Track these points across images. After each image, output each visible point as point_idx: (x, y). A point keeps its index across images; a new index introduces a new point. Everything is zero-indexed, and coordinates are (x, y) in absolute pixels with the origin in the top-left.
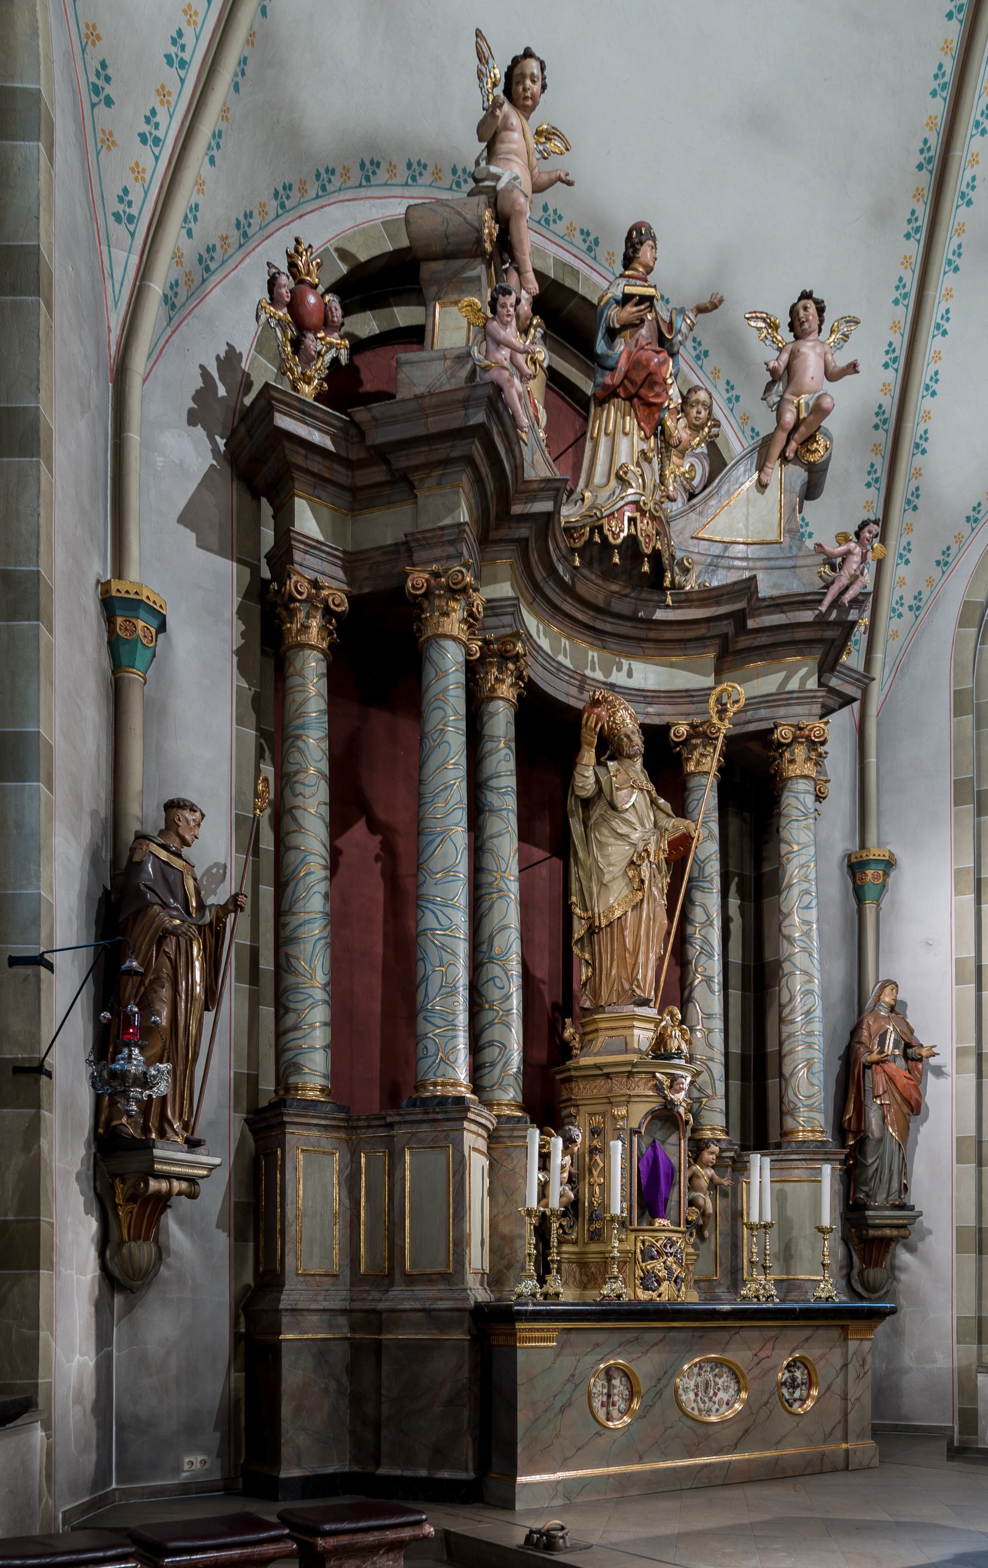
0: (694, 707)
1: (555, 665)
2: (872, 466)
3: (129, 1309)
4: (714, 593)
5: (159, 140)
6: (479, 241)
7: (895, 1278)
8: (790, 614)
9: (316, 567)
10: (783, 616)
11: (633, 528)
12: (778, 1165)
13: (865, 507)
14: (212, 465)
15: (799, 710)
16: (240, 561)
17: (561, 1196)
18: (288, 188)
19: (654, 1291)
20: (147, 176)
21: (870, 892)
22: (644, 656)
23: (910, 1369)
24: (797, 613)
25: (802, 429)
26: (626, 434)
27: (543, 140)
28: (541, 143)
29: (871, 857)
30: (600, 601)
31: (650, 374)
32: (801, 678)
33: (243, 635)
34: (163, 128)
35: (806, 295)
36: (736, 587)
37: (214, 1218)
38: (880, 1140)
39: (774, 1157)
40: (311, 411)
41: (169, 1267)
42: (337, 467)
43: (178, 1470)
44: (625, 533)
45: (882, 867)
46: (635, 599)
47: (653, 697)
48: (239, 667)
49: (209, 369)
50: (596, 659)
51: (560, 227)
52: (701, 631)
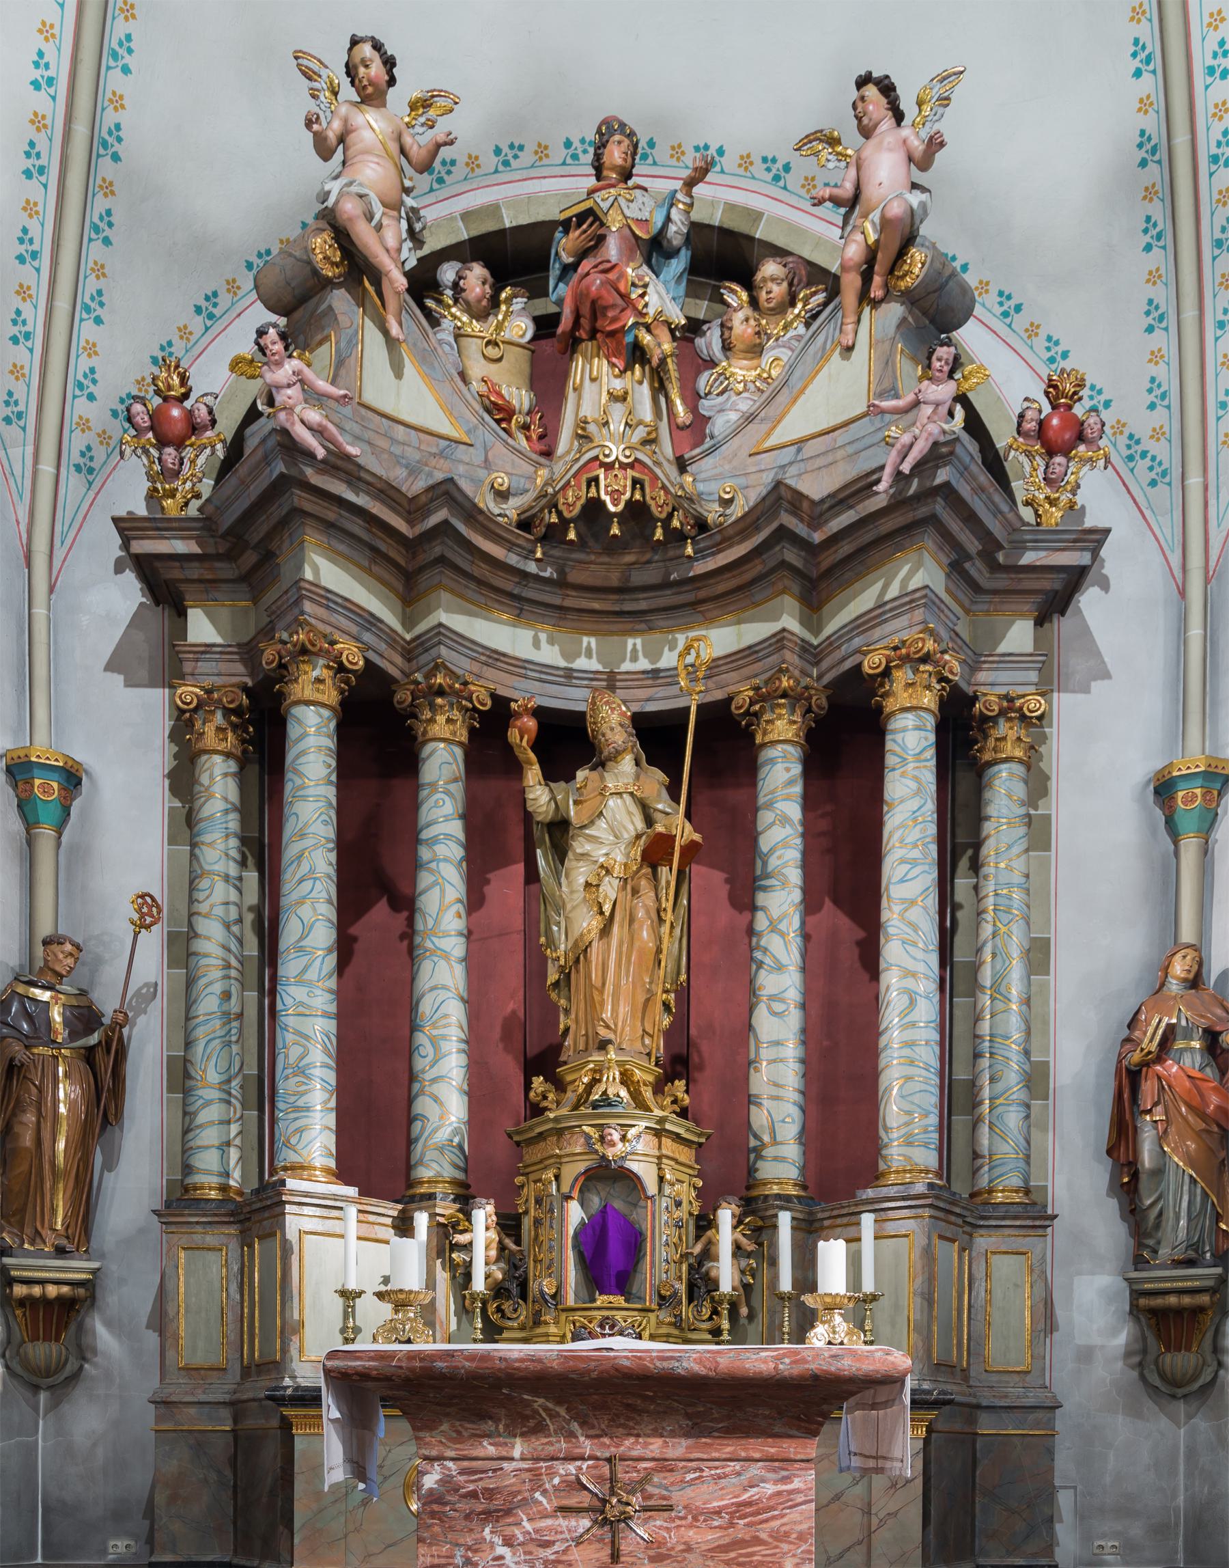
1: (561, 673)
3: (55, 1405)
4: (749, 520)
5: (30, 333)
6: (315, 272)
8: (860, 507)
10: (852, 512)
12: (362, 1217)
14: (141, 604)
18: (212, 297)
22: (710, 621)
24: (867, 502)
25: (880, 256)
27: (421, 111)
29: (1175, 774)
30: (614, 579)
31: (593, 302)
32: (903, 580)
33: (176, 756)
34: (30, 322)
35: (863, 82)
36: (768, 503)
37: (144, 1320)
38: (1158, 1172)
39: (361, 1207)
42: (218, 565)
43: (104, 1552)
44: (583, 501)
45: (1199, 782)
46: (664, 561)
48: (171, 789)
50: (639, 647)
52: (756, 568)
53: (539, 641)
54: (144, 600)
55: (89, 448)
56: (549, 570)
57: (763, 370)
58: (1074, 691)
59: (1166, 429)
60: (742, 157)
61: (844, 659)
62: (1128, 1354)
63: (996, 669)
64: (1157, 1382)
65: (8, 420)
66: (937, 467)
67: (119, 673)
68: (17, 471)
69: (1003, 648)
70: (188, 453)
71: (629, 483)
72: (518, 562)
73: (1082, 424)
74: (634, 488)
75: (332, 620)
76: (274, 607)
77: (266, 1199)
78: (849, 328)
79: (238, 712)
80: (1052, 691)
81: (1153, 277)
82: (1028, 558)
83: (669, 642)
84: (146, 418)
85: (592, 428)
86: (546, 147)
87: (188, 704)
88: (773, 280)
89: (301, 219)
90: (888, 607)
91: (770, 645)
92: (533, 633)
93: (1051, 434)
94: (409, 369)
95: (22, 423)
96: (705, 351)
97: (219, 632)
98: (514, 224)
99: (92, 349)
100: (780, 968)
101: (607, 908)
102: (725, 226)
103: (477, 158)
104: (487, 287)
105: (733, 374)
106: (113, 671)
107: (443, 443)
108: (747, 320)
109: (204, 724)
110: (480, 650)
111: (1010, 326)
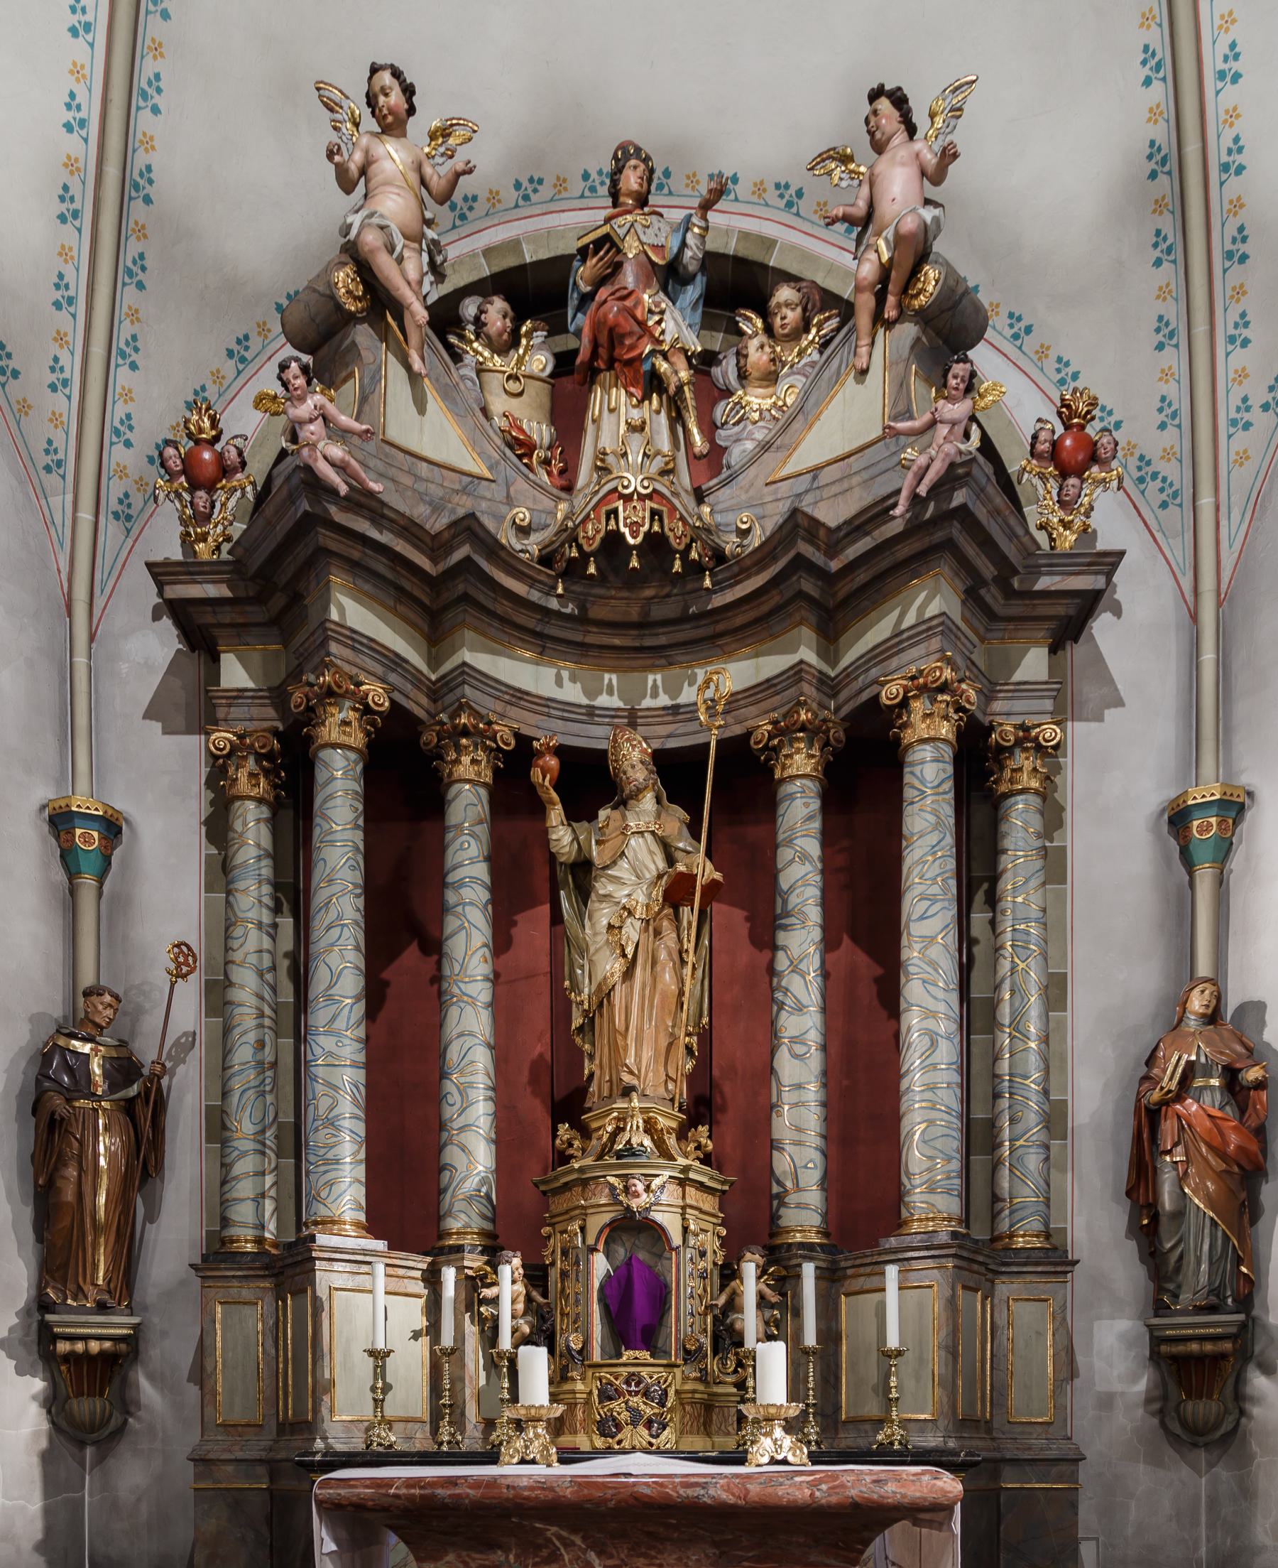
0: (778, 697)
3: (100, 1459)
7: (1242, 1412)
8: (876, 533)
9: (242, 716)
10: (868, 539)
11: (612, 522)
14: (178, 651)
15: (914, 653)
17: (513, 1333)
18: (243, 340)
19: (613, 1437)
20: (65, 419)
21: (1202, 854)
22: (728, 654)
23: (1265, 1547)
24: (883, 528)
25: (893, 274)
26: (611, 411)
28: (441, 145)
30: (634, 614)
31: (611, 330)
35: (874, 95)
36: (784, 531)
37: (186, 1373)
38: (1179, 1215)
40: (197, 569)
41: (139, 1419)
44: (602, 534)
45: (1214, 810)
46: (683, 594)
48: (207, 836)
50: (659, 683)
52: (774, 599)
54: (181, 646)
55: (127, 495)
56: (571, 606)
58: (1087, 720)
59: (1177, 449)
60: (755, 185)
61: (861, 691)
62: (1149, 1401)
64: (1177, 1429)
67: (157, 720)
69: (1018, 676)
71: (647, 514)
72: (540, 599)
74: (652, 520)
75: (358, 661)
76: (301, 650)
77: (297, 1255)
78: (863, 351)
79: (270, 756)
82: (1044, 583)
85: (611, 459)
87: (221, 750)
88: (787, 305)
90: (905, 635)
91: (788, 678)
93: (1064, 455)
94: (434, 403)
95: (61, 471)
98: (534, 259)
100: (800, 1008)
101: (630, 951)
102: (740, 254)
104: (508, 320)
105: (748, 403)
106: (151, 719)
107: (466, 479)
108: (762, 347)
109: (237, 770)
111: (1020, 348)
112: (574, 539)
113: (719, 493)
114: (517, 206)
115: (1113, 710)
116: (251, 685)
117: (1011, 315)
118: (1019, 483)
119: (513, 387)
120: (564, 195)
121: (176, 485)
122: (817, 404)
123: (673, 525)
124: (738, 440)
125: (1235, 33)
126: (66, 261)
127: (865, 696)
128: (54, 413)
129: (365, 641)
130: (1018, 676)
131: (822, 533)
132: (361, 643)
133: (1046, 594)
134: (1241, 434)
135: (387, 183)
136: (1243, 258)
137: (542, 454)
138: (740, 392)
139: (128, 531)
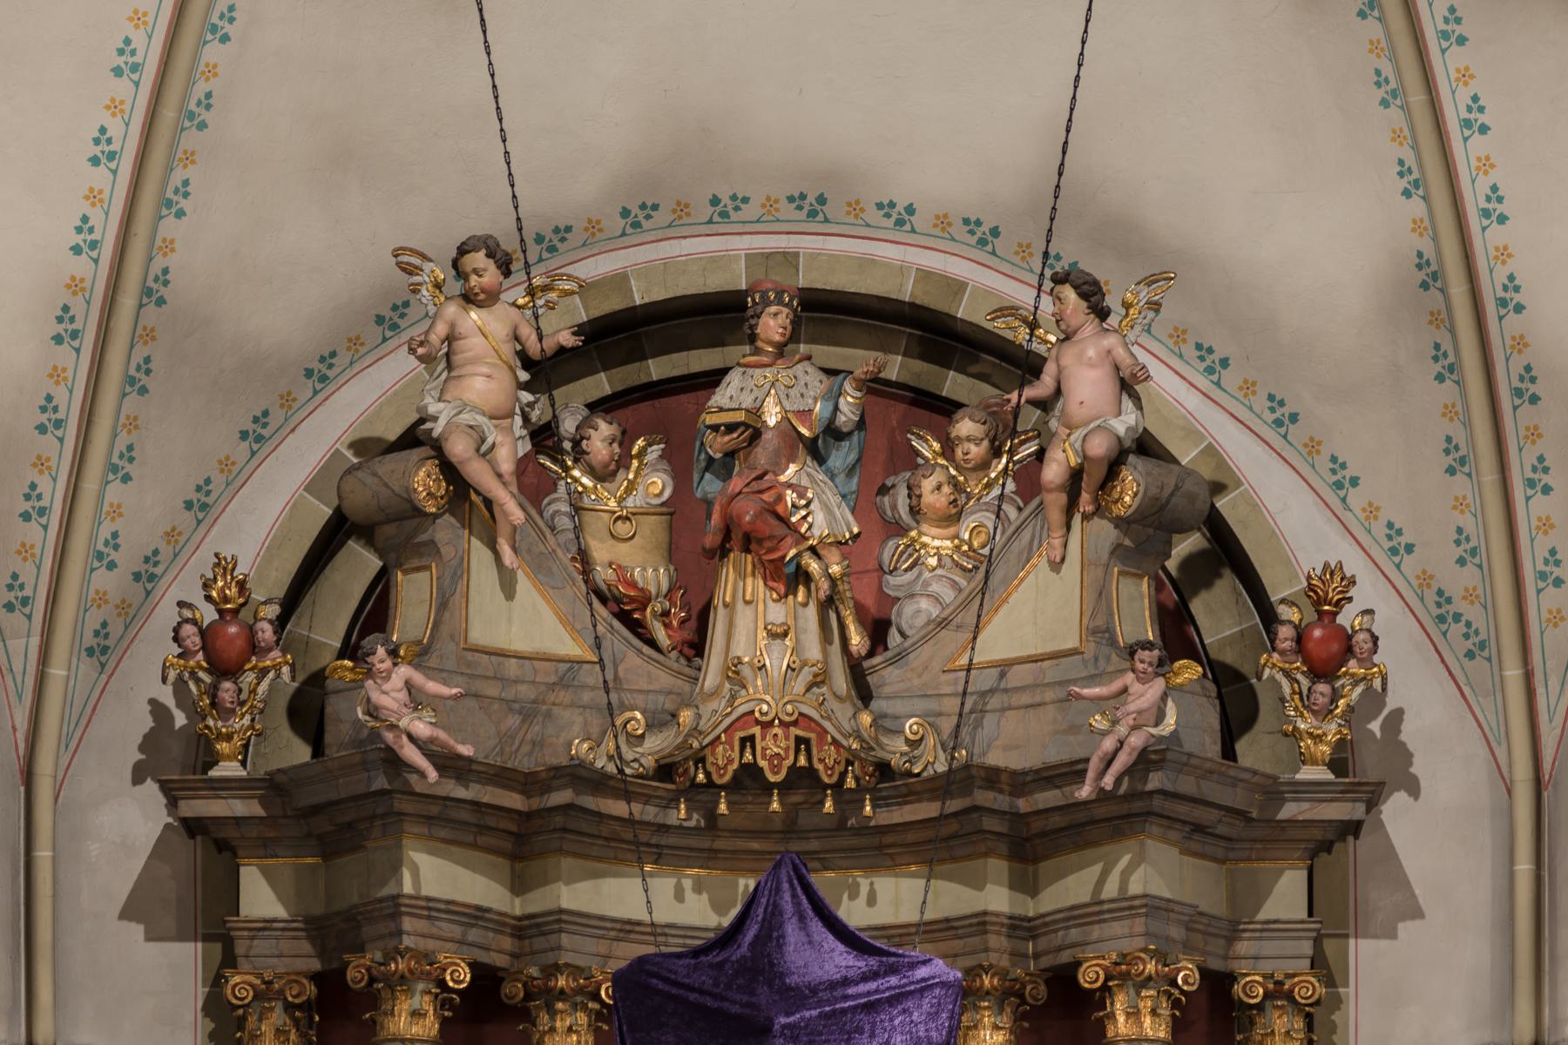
0: (960, 943)
2: (1437, 346)
9: (266, 952)
10: (1057, 792)
13: (1444, 415)
14: (167, 826)
16: (206, 938)
18: (261, 419)
20: (37, 551)
26: (748, 603)
32: (1123, 873)
44: (735, 766)
47: (901, 935)
49: (161, 700)
51: (751, 211)
53: (683, 890)
54: (170, 820)
55: (104, 625)
56: (695, 816)
57: (962, 541)
58: (1376, 937)
59: (1480, 591)
60: (937, 217)
61: (1060, 949)
63: (1260, 939)
65: (9, 607)
66: (1148, 770)
67: (138, 922)
68: (18, 665)
69: (1261, 916)
70: (249, 678)
71: (792, 744)
72: (656, 815)
73: (1350, 638)
74: (797, 751)
75: (434, 931)
78: (1057, 542)
79: (306, 1007)
80: (1347, 936)
81: (1448, 412)
82: (1289, 811)
83: (849, 887)
84: (197, 640)
85: (746, 672)
86: (687, 206)
87: (242, 999)
88: (969, 439)
89: (374, 312)
90: (1106, 907)
91: (971, 925)
92: (673, 881)
93: (1310, 645)
94: (523, 584)
95: (27, 610)
96: (889, 513)
97: (281, 898)
98: (647, 300)
99: (116, 512)
102: (918, 302)
103: (598, 222)
104: (615, 445)
105: (925, 545)
106: (130, 919)
107: (563, 667)
108: (939, 488)
109: (260, 1020)
110: (608, 925)
111: (1285, 437)
112: (700, 760)
113: (885, 673)
114: (624, 234)
115: (1409, 924)
116: (279, 911)
117: (1271, 398)
118: (1259, 678)
119: (623, 529)
120: (686, 220)
121: (192, 663)
122: (1006, 581)
123: (822, 755)
124: (912, 596)
125: (1494, 177)
126: (57, 383)
127: (1065, 957)
128: (23, 545)
129: (443, 906)
130: (1261, 916)
131: (1004, 777)
132: (439, 910)
133: (1291, 822)
134: (1551, 590)
135: (474, 361)
136: (1534, 399)
137: (658, 608)
138: (913, 533)
139: (103, 666)
